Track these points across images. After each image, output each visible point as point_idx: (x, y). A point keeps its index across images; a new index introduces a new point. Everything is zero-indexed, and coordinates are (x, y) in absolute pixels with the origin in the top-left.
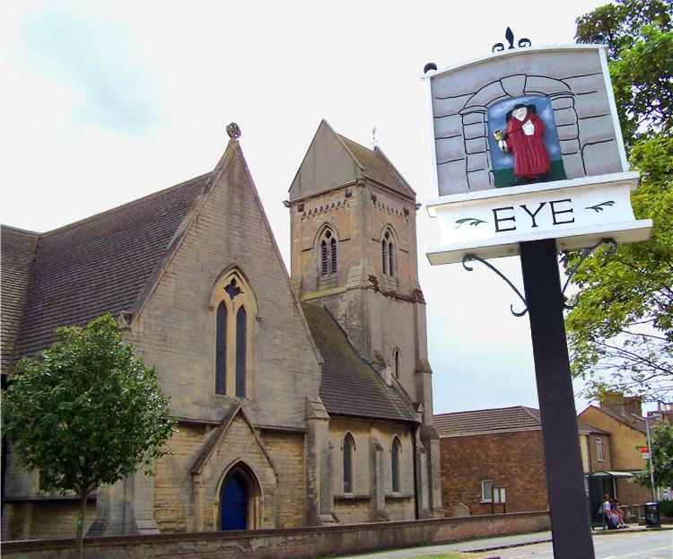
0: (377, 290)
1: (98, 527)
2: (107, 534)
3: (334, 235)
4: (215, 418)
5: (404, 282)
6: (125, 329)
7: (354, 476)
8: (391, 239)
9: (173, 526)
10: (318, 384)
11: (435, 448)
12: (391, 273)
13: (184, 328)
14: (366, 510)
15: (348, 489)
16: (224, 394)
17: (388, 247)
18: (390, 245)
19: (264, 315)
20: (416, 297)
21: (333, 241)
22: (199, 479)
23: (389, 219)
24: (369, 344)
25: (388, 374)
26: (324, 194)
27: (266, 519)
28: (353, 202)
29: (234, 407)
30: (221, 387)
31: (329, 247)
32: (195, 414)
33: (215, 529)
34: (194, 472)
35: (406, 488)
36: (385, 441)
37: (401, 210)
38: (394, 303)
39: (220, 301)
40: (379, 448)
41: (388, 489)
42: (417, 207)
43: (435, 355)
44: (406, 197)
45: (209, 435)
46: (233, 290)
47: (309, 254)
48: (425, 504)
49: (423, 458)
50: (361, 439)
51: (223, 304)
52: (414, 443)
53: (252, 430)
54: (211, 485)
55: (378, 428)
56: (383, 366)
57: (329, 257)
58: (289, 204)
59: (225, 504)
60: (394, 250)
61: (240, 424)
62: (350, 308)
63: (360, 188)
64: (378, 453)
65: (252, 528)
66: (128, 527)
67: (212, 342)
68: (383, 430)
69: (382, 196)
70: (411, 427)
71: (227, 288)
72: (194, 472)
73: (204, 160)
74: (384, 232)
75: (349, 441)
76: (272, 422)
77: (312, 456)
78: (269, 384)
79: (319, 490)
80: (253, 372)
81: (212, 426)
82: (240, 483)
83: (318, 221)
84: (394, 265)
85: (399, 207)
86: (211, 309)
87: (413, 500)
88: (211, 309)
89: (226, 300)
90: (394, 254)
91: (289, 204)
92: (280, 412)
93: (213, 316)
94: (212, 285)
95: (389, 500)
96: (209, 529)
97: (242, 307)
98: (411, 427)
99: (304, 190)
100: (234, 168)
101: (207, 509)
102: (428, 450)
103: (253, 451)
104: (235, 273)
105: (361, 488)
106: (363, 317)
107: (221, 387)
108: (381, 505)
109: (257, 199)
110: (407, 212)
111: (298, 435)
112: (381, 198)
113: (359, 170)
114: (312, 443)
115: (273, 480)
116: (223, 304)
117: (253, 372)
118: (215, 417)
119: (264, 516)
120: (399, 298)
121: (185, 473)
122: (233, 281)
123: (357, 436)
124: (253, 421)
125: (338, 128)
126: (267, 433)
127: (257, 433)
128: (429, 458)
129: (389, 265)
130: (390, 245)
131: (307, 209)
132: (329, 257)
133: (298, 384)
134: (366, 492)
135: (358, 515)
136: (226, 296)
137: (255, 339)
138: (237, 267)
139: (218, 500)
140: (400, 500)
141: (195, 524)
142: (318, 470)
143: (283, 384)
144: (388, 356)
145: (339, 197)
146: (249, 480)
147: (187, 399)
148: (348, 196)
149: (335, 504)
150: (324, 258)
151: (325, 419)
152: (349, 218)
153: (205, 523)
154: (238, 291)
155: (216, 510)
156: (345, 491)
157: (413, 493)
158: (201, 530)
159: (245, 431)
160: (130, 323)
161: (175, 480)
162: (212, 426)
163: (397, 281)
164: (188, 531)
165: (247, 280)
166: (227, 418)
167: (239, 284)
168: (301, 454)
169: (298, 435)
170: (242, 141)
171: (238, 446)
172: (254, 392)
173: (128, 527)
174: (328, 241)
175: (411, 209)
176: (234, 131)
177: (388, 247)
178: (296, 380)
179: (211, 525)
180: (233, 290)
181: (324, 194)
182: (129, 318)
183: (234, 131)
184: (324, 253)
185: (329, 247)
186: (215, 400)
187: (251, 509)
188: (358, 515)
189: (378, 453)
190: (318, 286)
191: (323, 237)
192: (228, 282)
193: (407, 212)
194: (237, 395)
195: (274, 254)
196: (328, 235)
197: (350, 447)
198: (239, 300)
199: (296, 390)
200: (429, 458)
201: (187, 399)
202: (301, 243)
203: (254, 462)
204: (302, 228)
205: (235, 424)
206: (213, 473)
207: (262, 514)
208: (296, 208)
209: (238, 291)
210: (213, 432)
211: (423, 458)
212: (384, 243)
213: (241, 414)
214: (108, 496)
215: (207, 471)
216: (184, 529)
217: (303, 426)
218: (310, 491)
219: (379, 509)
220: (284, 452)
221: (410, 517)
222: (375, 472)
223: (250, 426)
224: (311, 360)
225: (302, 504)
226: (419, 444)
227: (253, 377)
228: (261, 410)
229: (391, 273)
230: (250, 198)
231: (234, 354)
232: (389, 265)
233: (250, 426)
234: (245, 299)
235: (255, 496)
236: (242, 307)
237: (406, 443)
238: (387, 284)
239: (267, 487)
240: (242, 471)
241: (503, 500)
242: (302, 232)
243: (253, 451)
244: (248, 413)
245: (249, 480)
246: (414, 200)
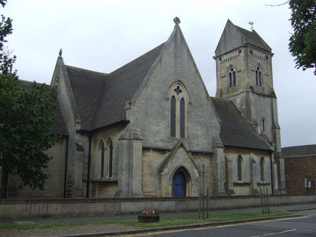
0: (253, 92)
1: (118, 193)
2: (122, 196)
3: (234, 70)
4: (170, 147)
5: (266, 88)
6: (128, 108)
7: (243, 174)
8: (260, 70)
9: (151, 194)
10: (218, 132)
11: (282, 161)
12: (260, 85)
13: (155, 108)
14: (249, 189)
15: (240, 179)
16: (175, 136)
17: (258, 73)
18: (260, 73)
19: (193, 101)
20: (272, 95)
21: (234, 72)
22: (163, 173)
23: (259, 61)
24: (250, 116)
25: (259, 129)
26: (229, 52)
27: (194, 192)
28: (242, 54)
29: (179, 142)
30: (173, 133)
31: (232, 75)
32: (161, 145)
33: (170, 196)
34: (160, 170)
35: (268, 180)
36: (257, 158)
37: (264, 57)
38: (262, 98)
39: (172, 96)
40: (254, 161)
41: (258, 179)
42: (272, 55)
43: (281, 120)
44: (267, 51)
45: (167, 154)
46: (178, 91)
47: (224, 79)
48: (276, 187)
49: (275, 166)
50: (246, 158)
51: (173, 97)
52: (271, 160)
53: (187, 152)
54: (169, 176)
55: (253, 152)
56: (257, 125)
57: (233, 79)
58: (215, 58)
59: (175, 186)
60: (261, 75)
61: (181, 150)
62: (242, 101)
63: (245, 48)
64: (253, 164)
65: (187, 195)
66: (130, 194)
67: (168, 113)
68: (256, 154)
69: (255, 51)
70: (269, 152)
71: (175, 90)
72: (160, 170)
73: (163, 35)
74: (257, 67)
75: (240, 158)
76: (196, 149)
77: (217, 164)
78: (195, 132)
79: (219, 176)
80: (188, 126)
81: (169, 151)
82: (182, 175)
83: (227, 64)
84: (262, 81)
85: (264, 56)
86: (168, 99)
87: (270, 185)
88: (168, 99)
89: (175, 96)
90: (261, 77)
91: (215, 58)
92: (202, 144)
93: (169, 102)
94: (168, 89)
95: (259, 184)
96: (168, 196)
97: (182, 98)
98: (269, 152)
99: (221, 51)
100: (177, 36)
101: (167, 188)
102: (278, 163)
103: (188, 161)
104: (179, 83)
105: (246, 179)
106: (248, 105)
107: (173, 133)
108: (255, 187)
109: (188, 51)
110: (267, 58)
111: (210, 155)
112: (255, 52)
113: (244, 40)
114: (216, 159)
115: (198, 175)
116: (173, 97)
117: (188, 126)
118: (170, 147)
119: (193, 190)
120: (264, 96)
121: (155, 171)
122: (178, 87)
123: (243, 156)
124: (188, 149)
125: (235, 23)
126: (195, 153)
127: (190, 154)
128: (279, 167)
129: (259, 81)
130: (260, 73)
131: (222, 60)
132: (233, 79)
133: (210, 132)
134: (248, 180)
135: (245, 191)
136: (175, 94)
137: (188, 112)
138: (179, 81)
139: (171, 183)
140: (265, 185)
141: (161, 193)
142: (219, 170)
143: (203, 132)
144: (259, 121)
145: (234, 54)
146: (186, 174)
147: (157, 139)
148: (240, 52)
149: (233, 186)
150: (231, 80)
151: (222, 148)
152: (239, 61)
153: (165, 193)
154: (180, 91)
155: (170, 187)
156: (239, 180)
157: (271, 182)
158: (164, 196)
159: (184, 153)
160: (130, 106)
161: (152, 174)
162: (169, 151)
163: (263, 88)
164: (158, 197)
165: (184, 86)
166: (175, 147)
167: (181, 88)
168: (211, 163)
169: (210, 155)
170: (180, 25)
171: (181, 159)
172: (188, 135)
173: (130, 194)
174: (232, 72)
175: (269, 56)
176: (177, 20)
177: (258, 73)
178: (208, 130)
179: (168, 194)
180: (178, 91)
181: (229, 52)
182: (130, 104)
183: (177, 20)
184: (231, 78)
185: (232, 75)
186: (170, 139)
187: (188, 187)
188: (245, 191)
189: (253, 164)
190: (228, 91)
191: (230, 71)
192: (176, 87)
193: (267, 58)
194: (181, 137)
195: (197, 74)
196: (232, 70)
197: (240, 161)
198: (181, 95)
199: (208, 135)
200: (279, 167)
201: (157, 139)
202: (221, 74)
203: (188, 165)
204: (221, 67)
205: (179, 150)
206: (169, 170)
207: (193, 190)
208: (218, 59)
209: (180, 91)
210: (169, 153)
211: (275, 166)
212: (257, 72)
213: (182, 145)
214: (122, 180)
215: (166, 170)
216: (156, 195)
217: (212, 151)
218: (215, 180)
219: (254, 188)
220: (205, 162)
221: (270, 192)
222: (252, 172)
223: (186, 150)
224: (216, 122)
225: (212, 185)
226: (273, 160)
227: (188, 129)
228: (192, 143)
229: (260, 85)
230: (185, 50)
231: (179, 119)
232: (259, 81)
233: (186, 150)
234: (184, 94)
235: (189, 182)
236: (182, 98)
237: (267, 160)
238: (258, 89)
239: (195, 178)
240: (183, 170)
241: (310, 187)
242: (221, 69)
243: (188, 161)
244: (186, 145)
245: (186, 174)
246: (271, 52)
